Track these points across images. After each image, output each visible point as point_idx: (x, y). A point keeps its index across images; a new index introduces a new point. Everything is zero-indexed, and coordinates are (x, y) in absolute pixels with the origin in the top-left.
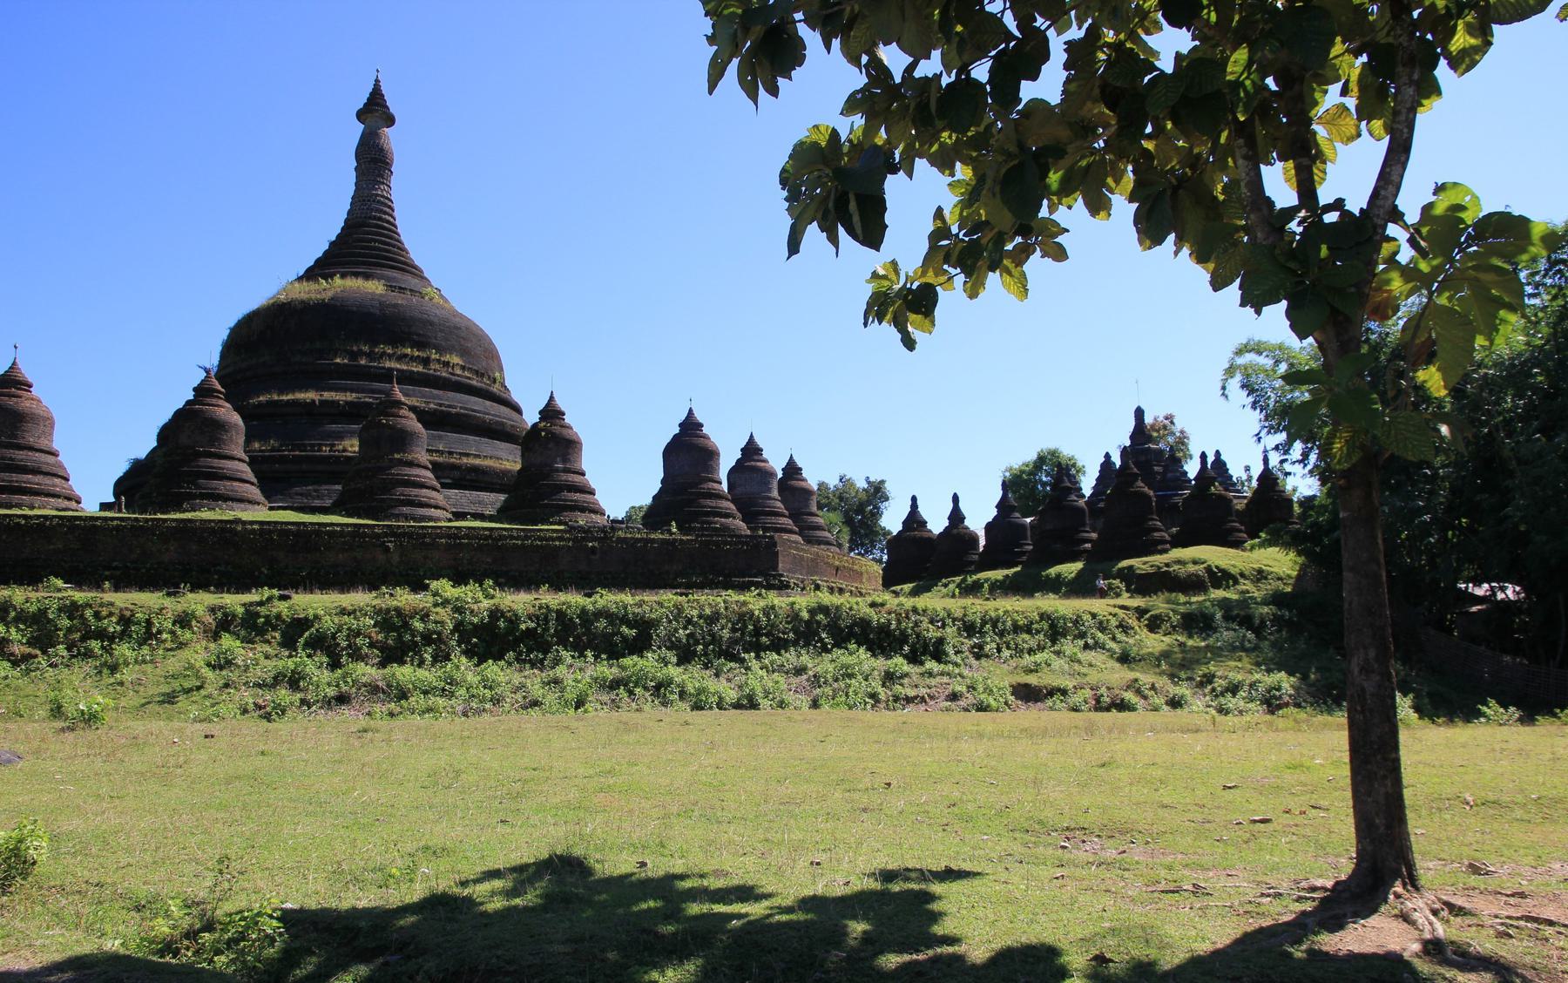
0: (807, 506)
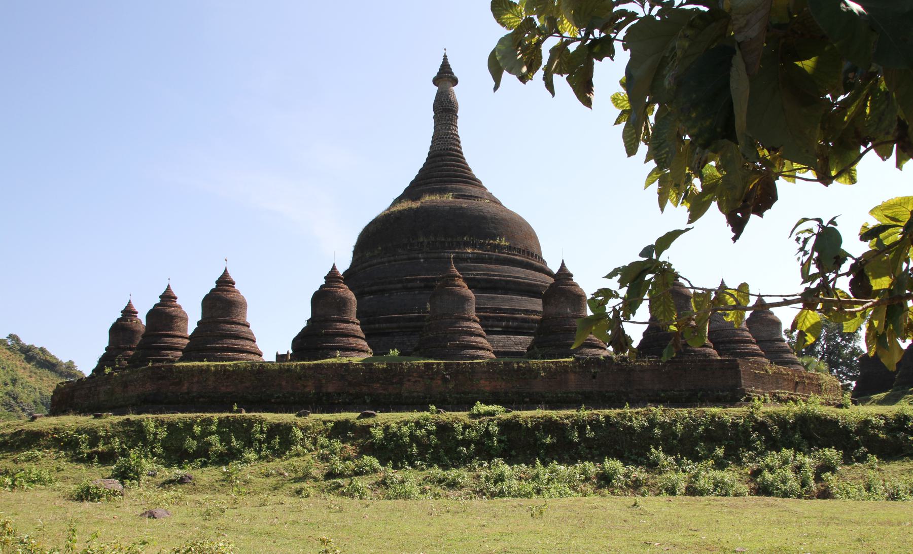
0: (464, 310)
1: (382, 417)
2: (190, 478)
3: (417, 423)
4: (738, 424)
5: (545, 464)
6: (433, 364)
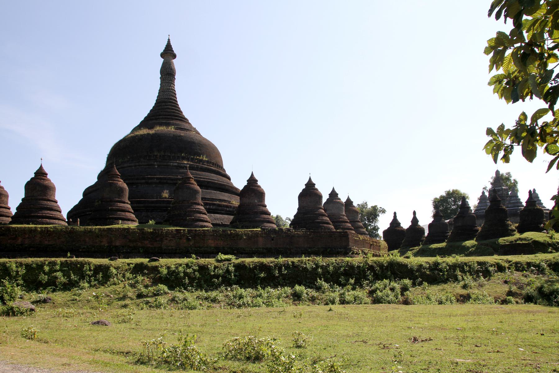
0: (196, 198)
1: (163, 261)
2: (50, 299)
3: (187, 265)
4: (360, 266)
5: (264, 289)
6: (181, 230)
